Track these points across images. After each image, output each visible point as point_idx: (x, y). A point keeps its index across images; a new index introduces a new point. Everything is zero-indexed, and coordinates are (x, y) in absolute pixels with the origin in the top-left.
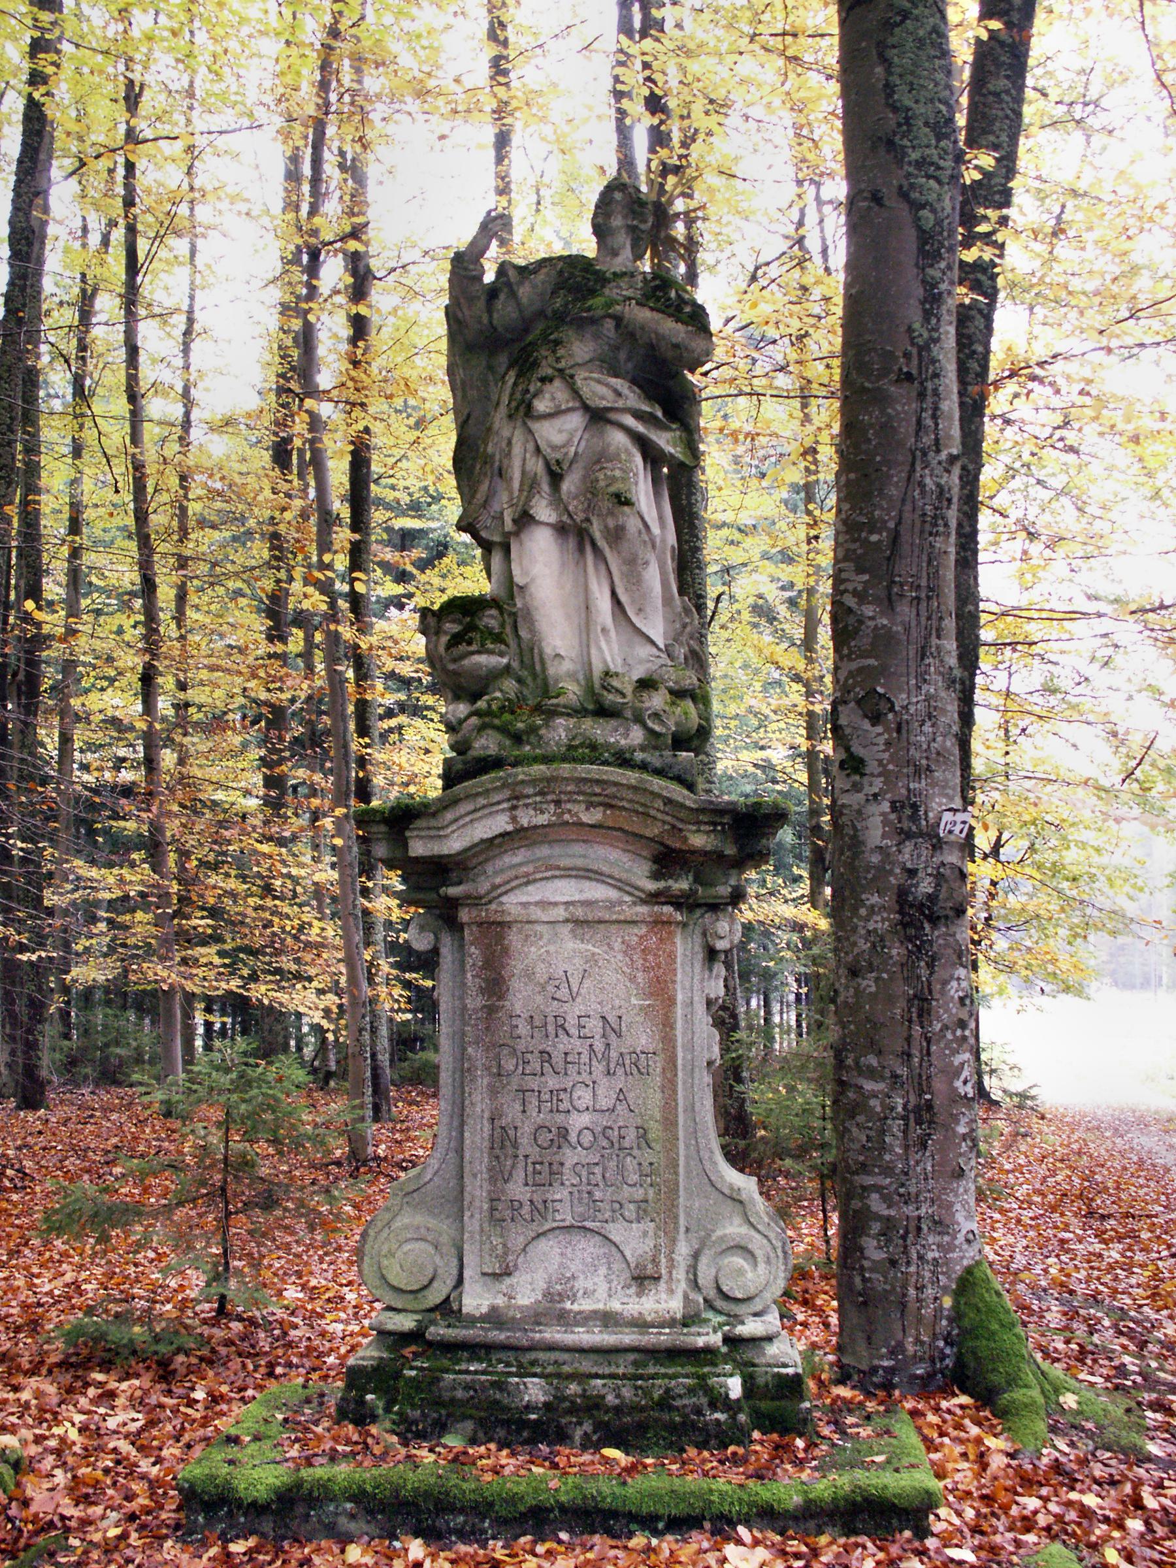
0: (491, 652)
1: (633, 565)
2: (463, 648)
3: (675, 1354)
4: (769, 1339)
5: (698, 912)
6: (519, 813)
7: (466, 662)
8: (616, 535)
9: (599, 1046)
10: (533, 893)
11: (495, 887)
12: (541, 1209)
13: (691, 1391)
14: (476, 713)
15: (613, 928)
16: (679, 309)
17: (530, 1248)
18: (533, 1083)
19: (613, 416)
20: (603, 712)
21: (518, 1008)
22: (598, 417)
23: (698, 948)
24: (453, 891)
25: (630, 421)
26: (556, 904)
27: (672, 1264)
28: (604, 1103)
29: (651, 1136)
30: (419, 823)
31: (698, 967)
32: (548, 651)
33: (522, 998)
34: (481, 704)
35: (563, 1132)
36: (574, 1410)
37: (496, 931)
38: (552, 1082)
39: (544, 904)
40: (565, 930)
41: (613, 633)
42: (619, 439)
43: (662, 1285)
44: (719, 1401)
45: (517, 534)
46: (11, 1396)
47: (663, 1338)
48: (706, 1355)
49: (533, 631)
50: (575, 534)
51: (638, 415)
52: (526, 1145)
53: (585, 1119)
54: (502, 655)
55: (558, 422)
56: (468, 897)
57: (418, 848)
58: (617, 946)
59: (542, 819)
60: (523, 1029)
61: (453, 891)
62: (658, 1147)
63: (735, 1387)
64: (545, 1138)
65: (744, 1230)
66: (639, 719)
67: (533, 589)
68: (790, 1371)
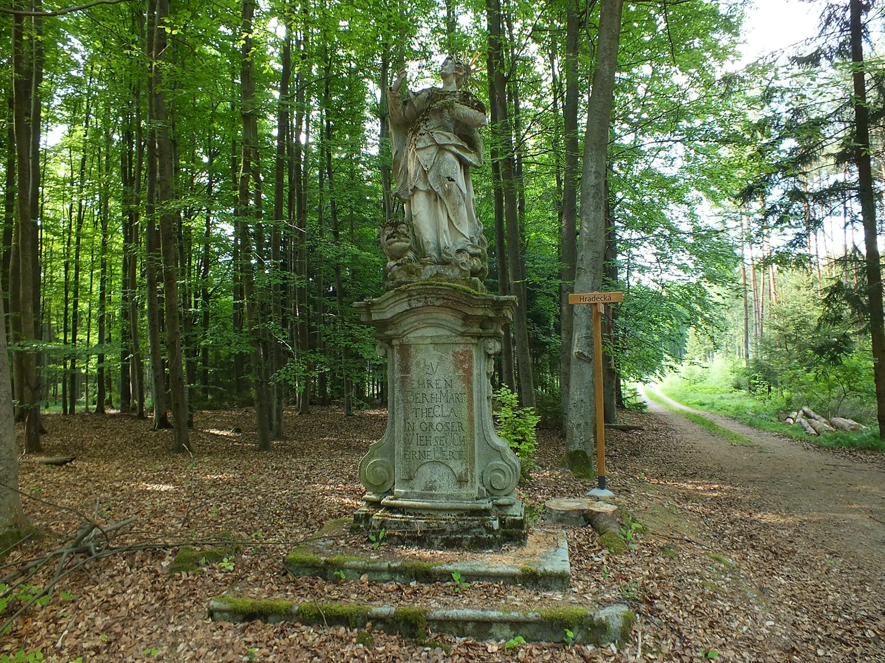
0: (402, 241)
1: (456, 207)
2: (392, 239)
3: (474, 512)
4: (511, 505)
5: (482, 339)
6: (412, 302)
7: (393, 245)
8: (448, 193)
9: (444, 391)
10: (419, 333)
11: (404, 331)
12: (423, 454)
13: (479, 526)
14: (398, 265)
15: (449, 346)
16: (472, 104)
17: (420, 470)
18: (419, 406)
19: (447, 147)
20: (446, 263)
21: (414, 377)
22: (441, 148)
23: (482, 353)
24: (389, 333)
25: (454, 149)
26: (427, 337)
27: (472, 476)
28: (446, 413)
29: (464, 426)
30: (375, 307)
31: (482, 360)
32: (425, 240)
33: (415, 373)
34: (399, 261)
35: (431, 425)
36: (434, 532)
37: (405, 350)
38: (426, 405)
39: (422, 337)
40: (431, 347)
41: (448, 233)
42: (450, 156)
43: (469, 484)
44: (490, 530)
45: (413, 195)
46: (508, 530)
47: (468, 505)
48: (486, 512)
49: (420, 233)
50: (433, 196)
51: (457, 146)
52: (418, 430)
53: (438, 420)
54: (407, 242)
55: (427, 151)
56: (395, 335)
57: (375, 317)
58: (451, 353)
59: (420, 304)
60: (415, 385)
61: (389, 333)
62: (466, 430)
63: (496, 524)
64: (424, 426)
65: (501, 463)
66: (457, 265)
67: (418, 216)
68: (518, 518)
